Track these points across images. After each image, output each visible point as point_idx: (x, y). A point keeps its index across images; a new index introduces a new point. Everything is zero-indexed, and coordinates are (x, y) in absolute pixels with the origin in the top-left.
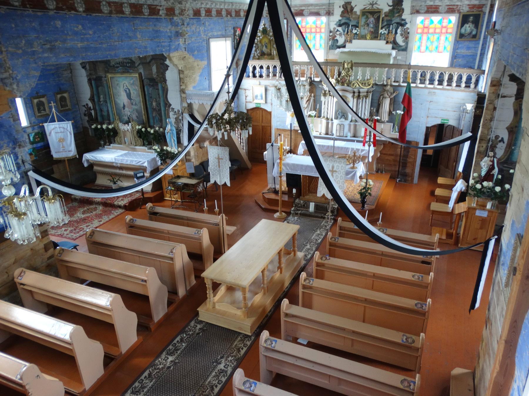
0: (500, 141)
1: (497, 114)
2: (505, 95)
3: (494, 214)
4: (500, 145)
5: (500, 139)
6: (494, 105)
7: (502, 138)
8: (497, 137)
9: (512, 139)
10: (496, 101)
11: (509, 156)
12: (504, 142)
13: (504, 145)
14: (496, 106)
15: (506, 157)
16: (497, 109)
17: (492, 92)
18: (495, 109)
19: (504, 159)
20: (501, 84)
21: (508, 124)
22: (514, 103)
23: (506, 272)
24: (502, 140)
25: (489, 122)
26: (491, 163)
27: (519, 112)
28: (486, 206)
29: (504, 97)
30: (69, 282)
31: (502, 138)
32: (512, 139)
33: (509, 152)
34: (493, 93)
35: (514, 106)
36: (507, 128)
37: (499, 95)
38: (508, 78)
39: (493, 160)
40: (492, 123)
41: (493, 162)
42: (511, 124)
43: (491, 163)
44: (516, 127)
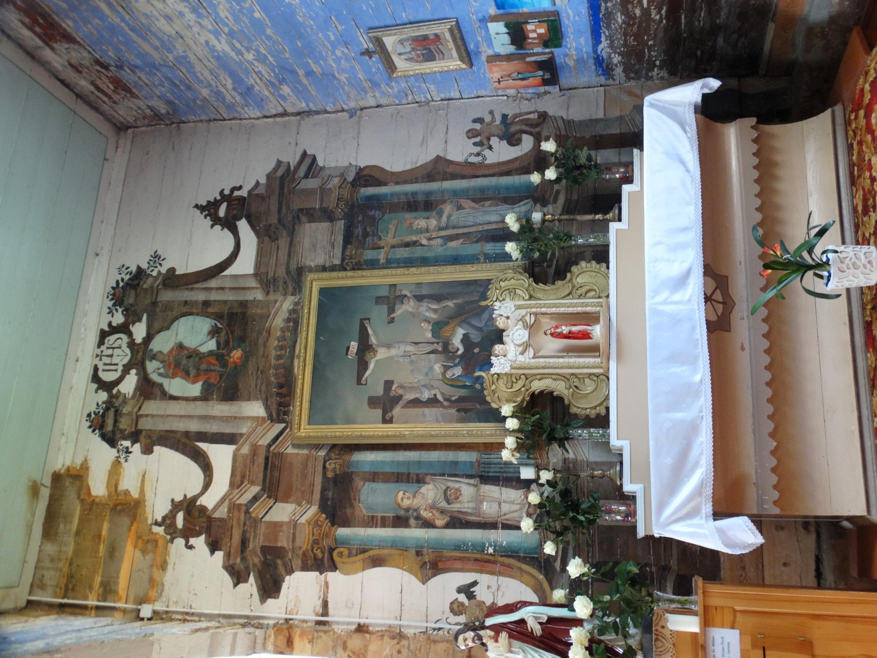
0: (471, 596)
1: (376, 618)
2: (319, 603)
3: (714, 601)
4: (483, 594)
5: (462, 598)
6: (350, 634)
7: (460, 590)
8: (456, 609)
9: (460, 559)
10: (335, 627)
11: (523, 560)
12: (475, 583)
13: (484, 579)
14: (353, 627)
15: (525, 567)
16: (362, 621)
17: (308, 646)
18: (361, 629)
19: (535, 572)
20: (287, 620)
21: (410, 581)
22: (346, 573)
23: (56, 65)
24: (467, 590)
25: (404, 642)
26: (504, 635)
27: (371, 553)
28: (696, 634)
29: (325, 604)
30: (782, 125)
31: (460, 590)
32: (460, 559)
33: (511, 561)
34: (311, 641)
35: (355, 572)
36: (424, 582)
37: (319, 623)
38: (270, 601)
39: (492, 627)
40: (409, 632)
41: (498, 629)
42: (410, 571)
43: (504, 635)
44: (418, 553)
